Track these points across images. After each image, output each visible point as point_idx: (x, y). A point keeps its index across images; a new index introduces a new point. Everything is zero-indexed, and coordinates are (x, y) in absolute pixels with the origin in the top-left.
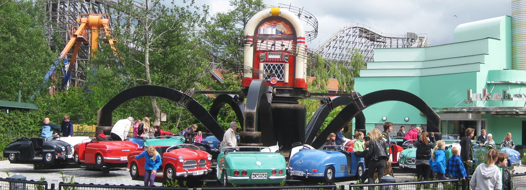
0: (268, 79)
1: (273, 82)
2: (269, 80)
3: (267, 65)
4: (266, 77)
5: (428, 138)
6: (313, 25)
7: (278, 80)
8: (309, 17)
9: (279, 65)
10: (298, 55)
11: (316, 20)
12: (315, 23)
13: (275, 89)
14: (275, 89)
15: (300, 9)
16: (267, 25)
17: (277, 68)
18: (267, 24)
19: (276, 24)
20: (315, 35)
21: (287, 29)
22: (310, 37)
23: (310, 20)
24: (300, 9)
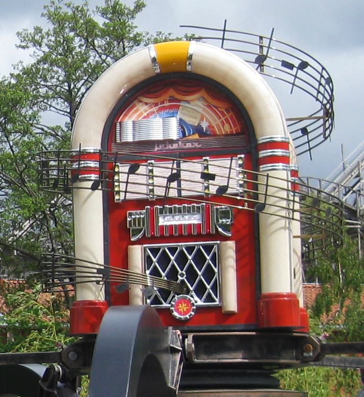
2: (165, 305)
5: (338, 358)
8: (296, 63)
11: (324, 74)
13: (191, 336)
14: (191, 336)
15: (261, 38)
16: (146, 107)
18: (146, 104)
19: (180, 101)
20: (325, 130)
22: (305, 139)
23: (301, 74)
24: (261, 38)
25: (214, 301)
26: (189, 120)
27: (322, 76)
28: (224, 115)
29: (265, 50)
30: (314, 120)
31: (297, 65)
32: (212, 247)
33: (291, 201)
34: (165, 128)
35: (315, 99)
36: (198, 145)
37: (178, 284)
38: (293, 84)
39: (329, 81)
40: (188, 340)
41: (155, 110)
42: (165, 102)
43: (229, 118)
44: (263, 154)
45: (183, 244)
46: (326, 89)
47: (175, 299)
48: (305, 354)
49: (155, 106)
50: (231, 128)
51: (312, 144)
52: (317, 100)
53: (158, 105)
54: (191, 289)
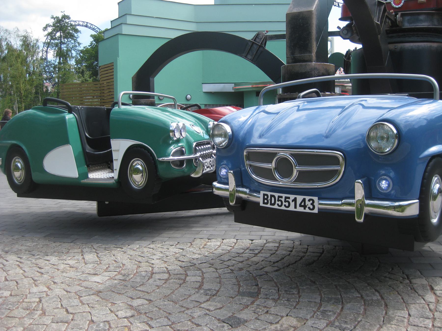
1: (396, 5)
13: (400, 14)
14: (400, 14)
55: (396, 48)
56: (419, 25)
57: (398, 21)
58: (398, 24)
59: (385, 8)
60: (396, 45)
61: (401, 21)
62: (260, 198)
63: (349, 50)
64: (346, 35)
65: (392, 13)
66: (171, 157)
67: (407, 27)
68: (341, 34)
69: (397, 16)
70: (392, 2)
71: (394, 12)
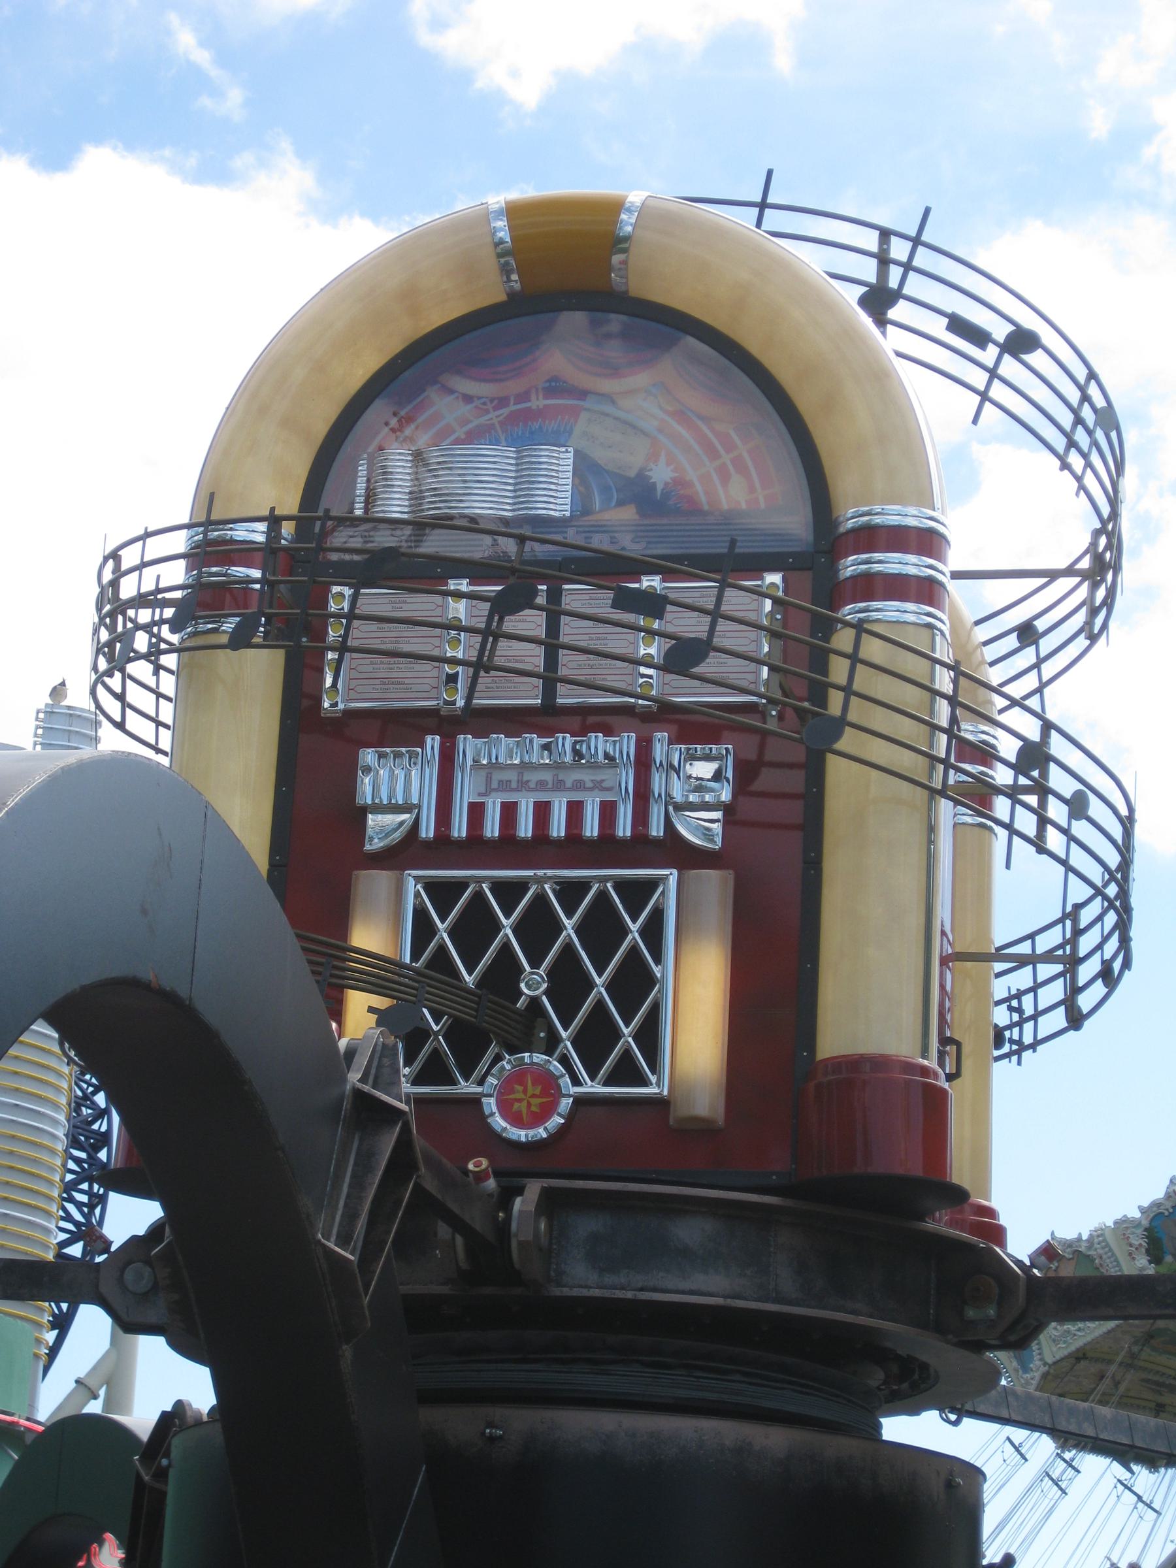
0: (453, 1082)
1: (517, 1120)
2: (466, 1087)
3: (443, 893)
4: (436, 1053)
5: (1109, 1416)
6: (1060, 443)
7: (592, 1087)
8: (1000, 331)
9: (603, 895)
10: (848, 741)
11: (1093, 391)
12: (1079, 421)
13: (533, 1189)
14: (533, 1189)
15: (885, 235)
16: (465, 410)
17: (578, 930)
18: (468, 399)
19: (583, 394)
20: (1094, 612)
21: (713, 453)
22: (1028, 657)
23: (1010, 367)
24: (885, 235)
25: (645, 1082)
26: (600, 455)
27: (1085, 398)
28: (730, 447)
29: (895, 273)
30: (1147, 1488)
31: (1001, 338)
32: (651, 885)
33: (943, 696)
34: (524, 481)
35: (1058, 463)
36: (633, 541)
37: (517, 1012)
38: (984, 396)
39: (1108, 419)
40: (523, 1202)
41: (495, 421)
42: (533, 397)
43: (746, 455)
44: (851, 566)
45: (550, 873)
46: (1095, 444)
47: (503, 1068)
48: (971, 1313)
49: (496, 408)
50: (752, 490)
51: (1048, 670)
52: (1065, 466)
53: (507, 405)
54: (564, 1034)
55: (492, 1439)
56: (670, 1286)
57: (520, 1243)
58: (517, 1266)
59: (404, 1145)
60: (498, 1412)
61: (544, 1241)
62: (213, 493)
63: (179, 1405)
64: (145, 1297)
65: (480, 1177)
66: (496, 1050)
67: (585, 1292)
68: (104, 1289)
69: (518, 1201)
70: (492, 1101)
71: (497, 1174)
